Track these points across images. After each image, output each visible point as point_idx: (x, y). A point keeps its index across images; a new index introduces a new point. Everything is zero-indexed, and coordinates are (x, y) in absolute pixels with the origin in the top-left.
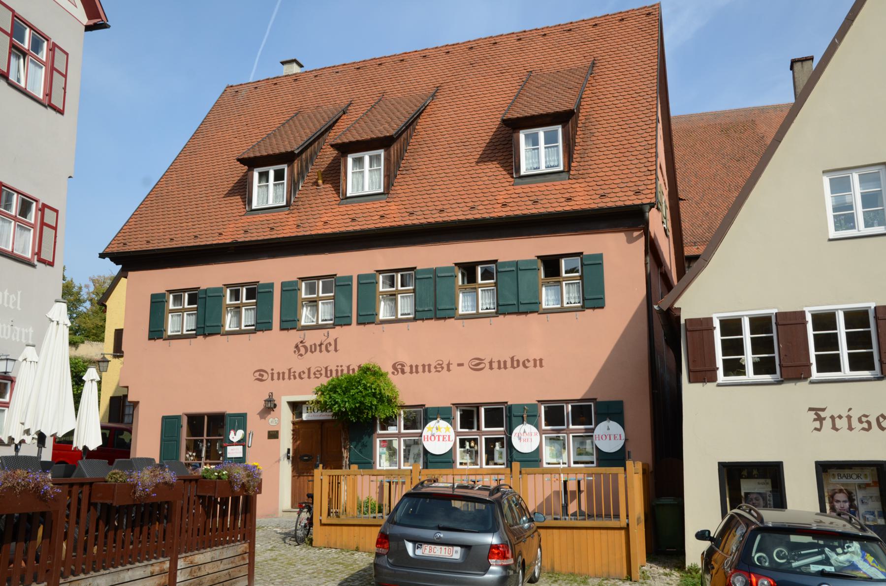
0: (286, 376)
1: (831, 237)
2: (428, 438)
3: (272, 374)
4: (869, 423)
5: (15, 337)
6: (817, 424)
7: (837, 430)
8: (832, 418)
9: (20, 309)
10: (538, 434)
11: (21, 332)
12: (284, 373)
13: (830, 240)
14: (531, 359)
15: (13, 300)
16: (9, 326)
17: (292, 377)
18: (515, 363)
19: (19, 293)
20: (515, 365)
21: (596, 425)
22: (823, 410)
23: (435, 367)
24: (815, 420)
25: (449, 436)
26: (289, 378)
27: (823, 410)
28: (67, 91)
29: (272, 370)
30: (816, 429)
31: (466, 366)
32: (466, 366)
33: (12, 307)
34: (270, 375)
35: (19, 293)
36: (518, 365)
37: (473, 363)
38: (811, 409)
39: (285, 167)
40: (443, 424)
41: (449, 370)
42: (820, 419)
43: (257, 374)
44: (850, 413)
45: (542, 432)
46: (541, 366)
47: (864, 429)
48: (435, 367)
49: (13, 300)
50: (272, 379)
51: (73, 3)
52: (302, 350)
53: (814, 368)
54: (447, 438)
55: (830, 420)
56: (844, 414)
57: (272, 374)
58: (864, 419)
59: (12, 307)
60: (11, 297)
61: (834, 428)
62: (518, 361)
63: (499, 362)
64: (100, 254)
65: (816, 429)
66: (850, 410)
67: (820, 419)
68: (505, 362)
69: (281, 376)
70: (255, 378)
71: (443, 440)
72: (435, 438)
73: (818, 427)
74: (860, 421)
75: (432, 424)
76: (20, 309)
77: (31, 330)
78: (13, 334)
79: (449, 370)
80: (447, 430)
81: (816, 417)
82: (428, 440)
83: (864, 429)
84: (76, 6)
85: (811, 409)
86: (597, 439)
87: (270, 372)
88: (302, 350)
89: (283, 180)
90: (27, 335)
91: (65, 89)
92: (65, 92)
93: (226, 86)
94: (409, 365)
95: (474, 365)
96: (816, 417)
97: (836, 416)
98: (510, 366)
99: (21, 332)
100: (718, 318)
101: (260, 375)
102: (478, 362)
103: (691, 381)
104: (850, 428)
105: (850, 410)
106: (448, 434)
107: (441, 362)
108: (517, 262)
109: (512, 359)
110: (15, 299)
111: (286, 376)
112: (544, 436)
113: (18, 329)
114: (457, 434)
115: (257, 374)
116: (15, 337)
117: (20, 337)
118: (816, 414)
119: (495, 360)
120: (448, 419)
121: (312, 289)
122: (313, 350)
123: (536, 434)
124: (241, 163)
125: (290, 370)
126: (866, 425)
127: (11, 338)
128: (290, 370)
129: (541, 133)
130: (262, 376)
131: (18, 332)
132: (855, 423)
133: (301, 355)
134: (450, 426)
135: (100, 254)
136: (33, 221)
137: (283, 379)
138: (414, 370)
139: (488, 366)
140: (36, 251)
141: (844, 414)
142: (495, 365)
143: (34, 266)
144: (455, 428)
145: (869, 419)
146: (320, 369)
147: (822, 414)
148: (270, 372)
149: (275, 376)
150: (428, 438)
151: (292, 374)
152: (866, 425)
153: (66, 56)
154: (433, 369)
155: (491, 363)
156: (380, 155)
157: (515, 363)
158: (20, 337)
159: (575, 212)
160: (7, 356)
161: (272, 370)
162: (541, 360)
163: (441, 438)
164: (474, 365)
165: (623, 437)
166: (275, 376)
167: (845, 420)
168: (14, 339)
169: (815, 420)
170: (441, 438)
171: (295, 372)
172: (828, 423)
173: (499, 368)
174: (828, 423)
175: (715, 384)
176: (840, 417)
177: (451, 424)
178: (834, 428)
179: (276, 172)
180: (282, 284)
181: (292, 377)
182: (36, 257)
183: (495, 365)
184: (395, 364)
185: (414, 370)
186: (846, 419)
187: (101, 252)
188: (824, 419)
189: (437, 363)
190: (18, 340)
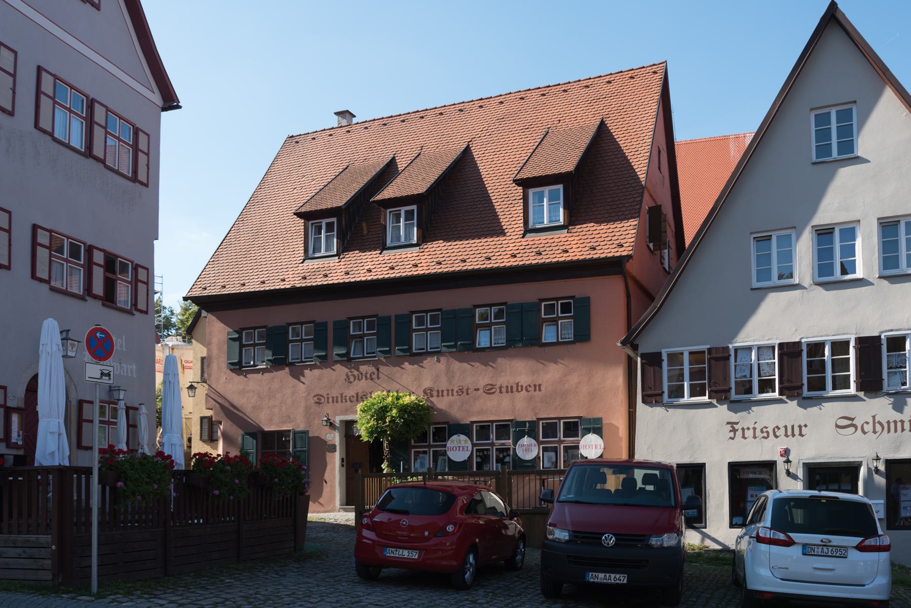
0: (339, 399)
1: (753, 287)
2: (450, 449)
3: (328, 398)
4: (768, 432)
5: (123, 372)
6: (732, 434)
7: (745, 438)
8: (743, 429)
9: (125, 350)
10: (537, 445)
11: (127, 368)
12: (337, 397)
13: (752, 289)
14: (532, 385)
15: (120, 343)
16: (118, 364)
17: (344, 401)
18: (520, 388)
19: (124, 337)
20: (520, 390)
21: (582, 437)
22: (737, 423)
23: (463, 392)
24: (731, 431)
25: (467, 447)
26: (342, 402)
27: (737, 423)
28: (150, 167)
29: (328, 394)
30: (731, 438)
31: (481, 390)
32: (481, 390)
33: (120, 349)
34: (326, 399)
35: (124, 337)
36: (522, 390)
37: (487, 388)
38: (728, 423)
39: (334, 220)
40: (463, 437)
41: (468, 394)
42: (734, 431)
43: (316, 399)
44: (756, 426)
45: (539, 443)
46: (540, 390)
47: (764, 437)
48: (457, 392)
49: (120, 343)
50: (328, 402)
51: (150, 88)
52: (352, 379)
53: (805, 388)
54: (466, 449)
55: (741, 431)
56: (751, 427)
57: (328, 398)
58: (765, 430)
59: (120, 349)
60: (118, 340)
61: (744, 437)
62: (522, 386)
63: (507, 387)
64: (183, 298)
65: (731, 438)
66: (756, 423)
67: (734, 431)
68: (512, 387)
69: (335, 400)
70: (314, 401)
71: (463, 451)
72: (456, 449)
73: (733, 436)
74: (762, 432)
75: (455, 437)
76: (125, 350)
77: (134, 367)
78: (122, 371)
79: (468, 394)
80: (466, 441)
81: (731, 429)
82: (451, 451)
83: (764, 437)
84: (154, 93)
85: (728, 423)
86: (582, 448)
87: (326, 396)
88: (352, 379)
89: (334, 232)
90: (132, 370)
91: (148, 165)
92: (148, 168)
93: (287, 136)
94: (436, 389)
95: (486, 390)
96: (731, 429)
97: (745, 428)
98: (516, 390)
99: (127, 368)
100: (666, 352)
101: (318, 399)
102: (490, 387)
103: (644, 401)
104: (755, 437)
105: (756, 423)
106: (466, 445)
107: (461, 388)
108: (522, 304)
109: (517, 384)
110: (121, 342)
111: (339, 399)
112: (541, 446)
113: (125, 366)
114: (474, 445)
115: (316, 399)
116: (123, 372)
117: (127, 373)
118: (732, 427)
119: (504, 385)
120: (469, 434)
121: (359, 326)
122: (360, 378)
123: (535, 446)
124: (298, 217)
125: (342, 395)
126: (765, 435)
127: (120, 373)
128: (342, 395)
129: (546, 190)
130: (320, 399)
131: (125, 368)
132: (758, 433)
133: (351, 382)
134: (468, 439)
135: (183, 298)
136: (130, 280)
137: (337, 402)
138: (440, 394)
139: (498, 391)
140: (134, 303)
141: (751, 427)
142: (504, 390)
143: (133, 314)
144: (472, 440)
145: (768, 430)
146: (365, 394)
147: (736, 427)
148: (326, 396)
149: (331, 400)
150: (450, 449)
151: (344, 398)
152: (765, 435)
153: (147, 137)
154: (455, 393)
155: (501, 388)
156: (413, 210)
157: (520, 388)
158: (127, 373)
159: (571, 262)
160: (119, 387)
161: (328, 394)
162: (540, 385)
163: (461, 449)
164: (486, 390)
165: (602, 446)
166: (331, 400)
167: (751, 431)
168: (122, 374)
169: (731, 431)
170: (461, 449)
171: (346, 396)
172: (739, 433)
173: (507, 392)
174: (739, 433)
175: (801, 398)
176: (748, 429)
177: (469, 437)
178: (744, 437)
179: (327, 224)
180: (334, 322)
181: (344, 401)
182: (134, 307)
183: (504, 390)
184: (426, 389)
185: (440, 394)
186: (752, 430)
187: (184, 296)
188: (737, 430)
189: (458, 388)
190: (126, 375)
